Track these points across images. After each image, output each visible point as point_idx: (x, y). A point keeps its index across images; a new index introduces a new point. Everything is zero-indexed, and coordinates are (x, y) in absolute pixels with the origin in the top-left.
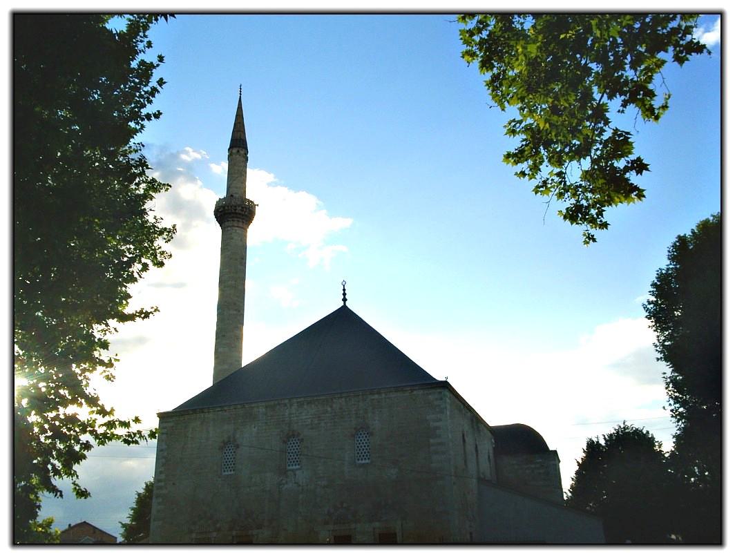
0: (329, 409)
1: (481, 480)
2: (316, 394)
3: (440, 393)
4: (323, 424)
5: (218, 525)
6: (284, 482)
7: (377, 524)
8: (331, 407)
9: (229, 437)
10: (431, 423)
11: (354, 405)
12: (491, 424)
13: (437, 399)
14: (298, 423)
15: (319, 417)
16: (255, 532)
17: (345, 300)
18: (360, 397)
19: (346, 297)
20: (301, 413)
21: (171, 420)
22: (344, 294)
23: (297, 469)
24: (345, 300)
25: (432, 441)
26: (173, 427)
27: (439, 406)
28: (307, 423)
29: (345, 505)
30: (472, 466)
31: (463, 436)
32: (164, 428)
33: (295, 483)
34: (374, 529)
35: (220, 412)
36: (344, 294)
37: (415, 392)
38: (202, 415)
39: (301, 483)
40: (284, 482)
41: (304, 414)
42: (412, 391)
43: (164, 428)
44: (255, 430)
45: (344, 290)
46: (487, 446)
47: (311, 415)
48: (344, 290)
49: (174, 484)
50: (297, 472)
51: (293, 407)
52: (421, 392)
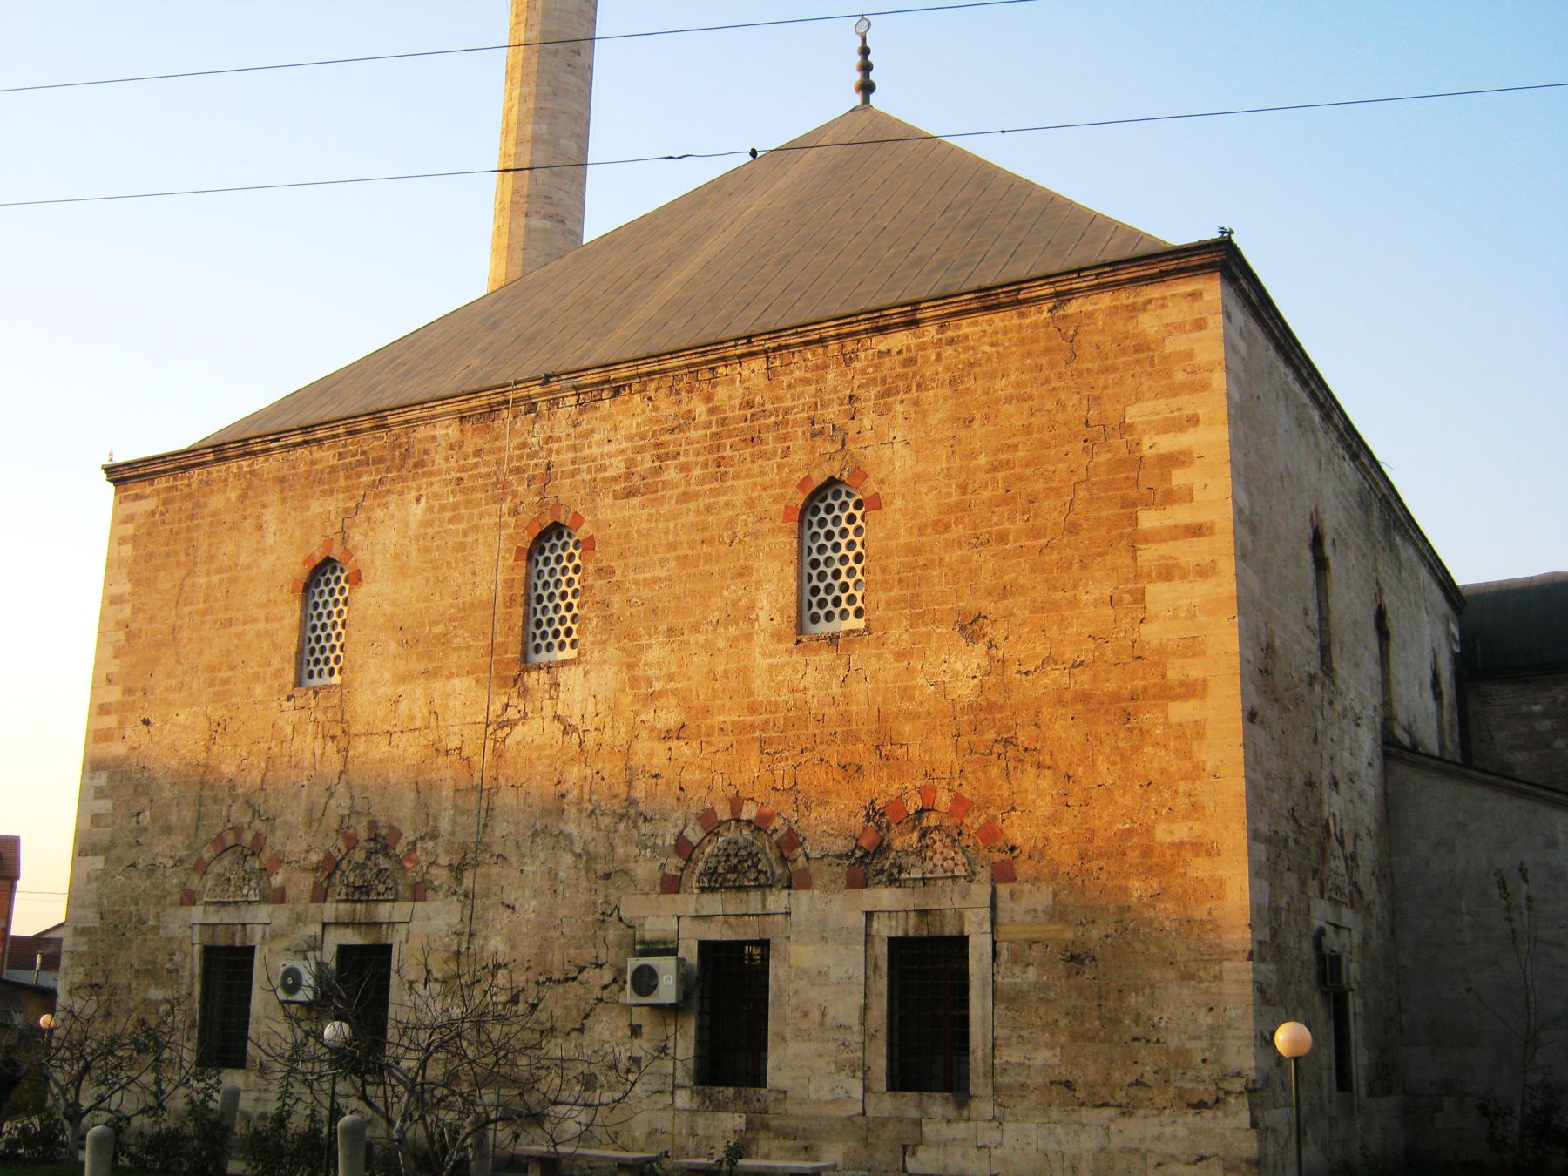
0: (700, 409)
1: (1396, 750)
2: (1361, 1058)
3: (1195, 295)
4: (671, 474)
5: (277, 880)
6: (512, 713)
7: (885, 897)
8: (709, 398)
9: (328, 543)
10: (1146, 442)
11: (807, 382)
12: (1465, 574)
13: (1179, 327)
14: (573, 474)
15: (658, 445)
16: (400, 911)
17: (867, 88)
18: (833, 346)
19: (873, 76)
20: (588, 434)
21: (148, 490)
22: (866, 68)
23: (564, 663)
24: (867, 88)
25: (1149, 520)
26: (153, 513)
27: (1190, 355)
28: (611, 473)
29: (749, 811)
30: (1357, 678)
31: (1317, 541)
32: (129, 519)
33: (557, 718)
34: (869, 915)
35: (304, 452)
36: (866, 68)
37: (1074, 306)
38: (245, 464)
39: (576, 721)
40: (512, 713)
41: (596, 437)
42: (1061, 298)
43: (129, 519)
44: (418, 511)
45: (865, 51)
46: (1426, 643)
47: (630, 438)
48: (865, 51)
49: (146, 722)
50: (564, 676)
51: (560, 412)
52: (1105, 300)
